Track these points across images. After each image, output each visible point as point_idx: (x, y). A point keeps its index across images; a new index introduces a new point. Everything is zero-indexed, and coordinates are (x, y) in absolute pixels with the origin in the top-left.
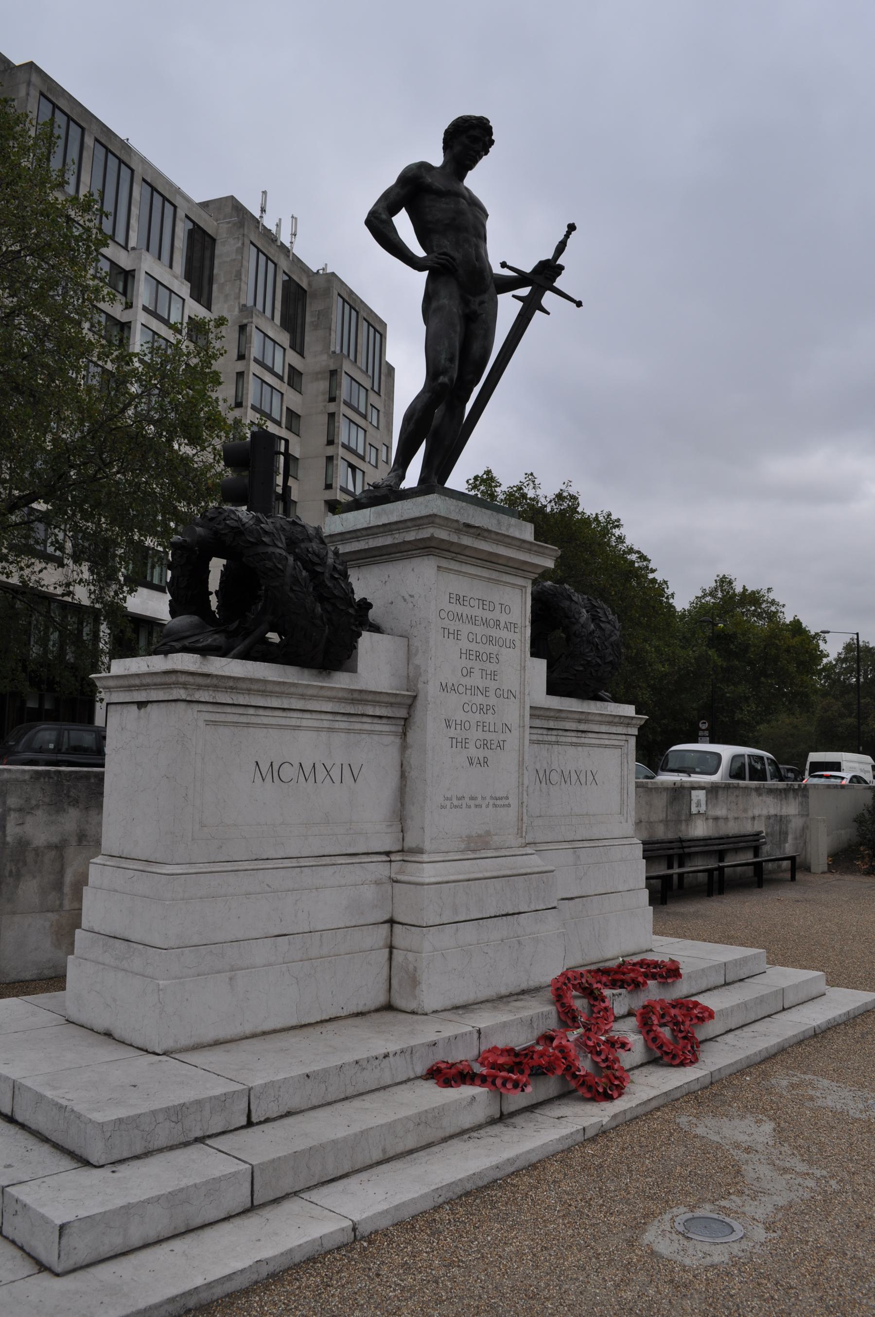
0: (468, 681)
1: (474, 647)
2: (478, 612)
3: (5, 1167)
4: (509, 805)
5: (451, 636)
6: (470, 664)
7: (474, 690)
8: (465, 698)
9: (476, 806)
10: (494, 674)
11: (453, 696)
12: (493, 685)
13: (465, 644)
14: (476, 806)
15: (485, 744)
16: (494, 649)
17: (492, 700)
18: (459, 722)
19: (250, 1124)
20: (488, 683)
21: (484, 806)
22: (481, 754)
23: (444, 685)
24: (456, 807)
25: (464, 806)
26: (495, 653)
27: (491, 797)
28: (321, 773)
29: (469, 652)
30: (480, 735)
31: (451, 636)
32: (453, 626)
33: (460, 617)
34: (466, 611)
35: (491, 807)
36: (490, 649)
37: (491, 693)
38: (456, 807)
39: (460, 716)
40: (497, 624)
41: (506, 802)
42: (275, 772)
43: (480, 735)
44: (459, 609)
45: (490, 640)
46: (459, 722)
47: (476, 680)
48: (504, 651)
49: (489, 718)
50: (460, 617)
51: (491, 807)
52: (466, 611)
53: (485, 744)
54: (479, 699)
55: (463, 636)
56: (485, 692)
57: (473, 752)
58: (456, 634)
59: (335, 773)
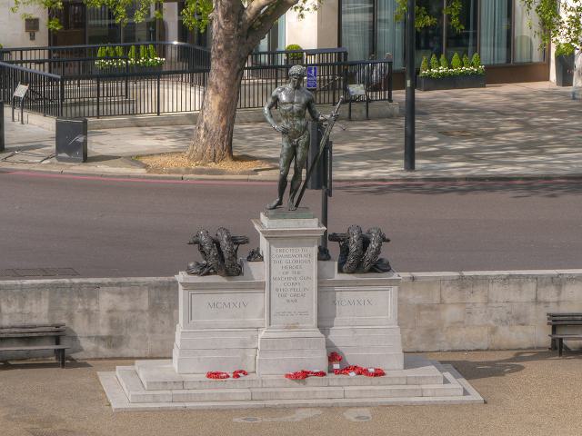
57: (288, 297)
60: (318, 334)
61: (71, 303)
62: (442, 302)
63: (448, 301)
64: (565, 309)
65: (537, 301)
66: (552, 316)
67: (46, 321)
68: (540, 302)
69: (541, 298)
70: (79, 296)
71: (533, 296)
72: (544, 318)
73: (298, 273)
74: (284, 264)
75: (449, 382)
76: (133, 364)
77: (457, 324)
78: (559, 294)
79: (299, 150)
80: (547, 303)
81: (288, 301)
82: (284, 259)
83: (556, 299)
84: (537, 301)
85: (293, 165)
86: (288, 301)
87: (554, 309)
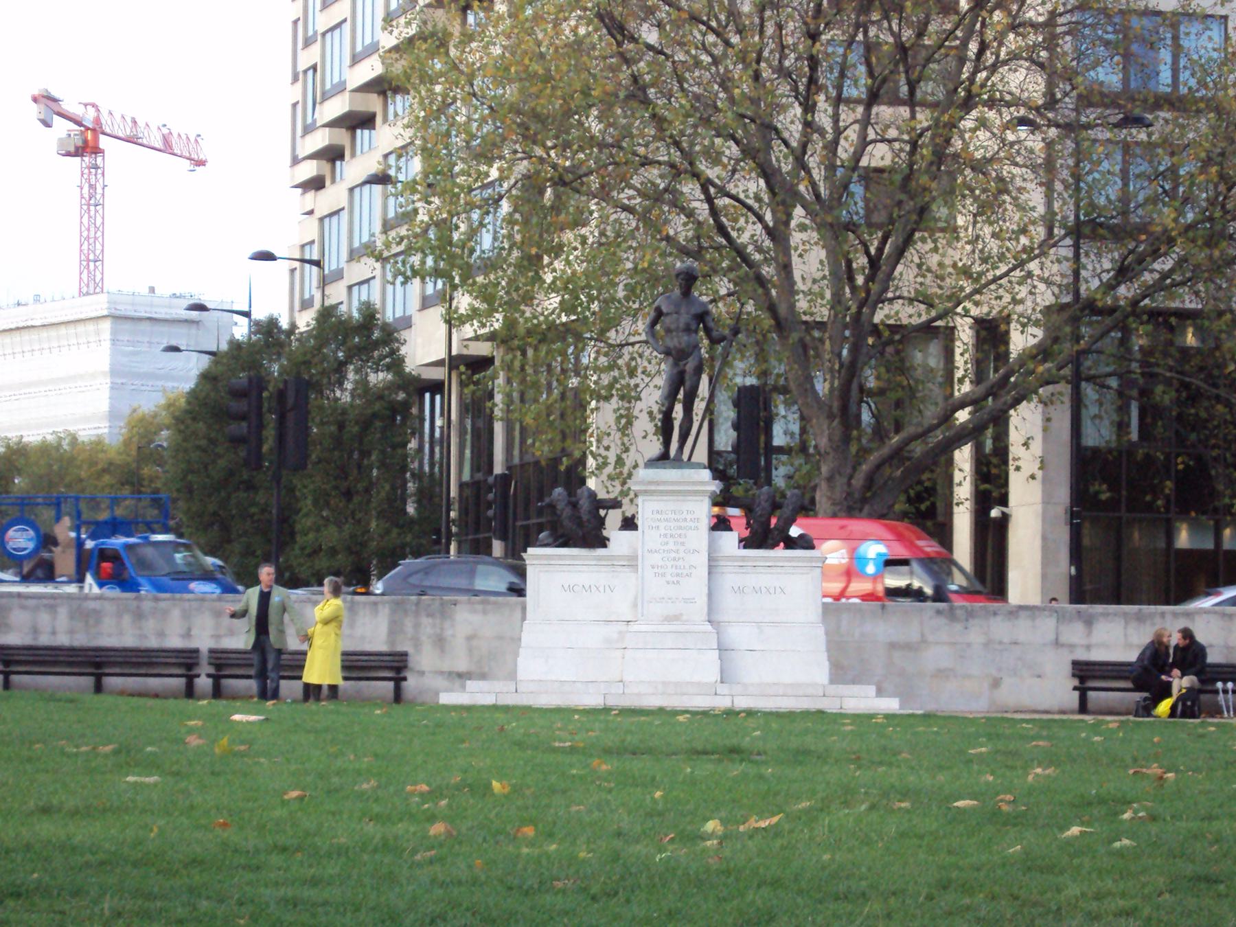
0: (666, 548)
1: (669, 532)
12: (682, 548)
15: (678, 575)
17: (682, 554)
28: (594, 589)
29: (665, 535)
45: (680, 528)
47: (671, 546)
49: (680, 563)
53: (678, 575)
54: (673, 555)
57: (669, 578)
59: (601, 589)
60: (709, 627)
61: (417, 626)
62: (924, 640)
63: (930, 638)
64: (1098, 655)
65: (1057, 643)
66: (1076, 664)
67: (382, 647)
68: (1063, 645)
69: (1064, 639)
70: (428, 615)
71: (1053, 637)
72: (1067, 669)
73: (683, 544)
74: (663, 531)
75: (1028, 448)
76: (463, 687)
77: (942, 674)
78: (1089, 634)
79: (687, 377)
80: (1072, 647)
82: (662, 525)
83: (1084, 642)
84: (1057, 643)
85: (681, 396)
87: (1082, 656)
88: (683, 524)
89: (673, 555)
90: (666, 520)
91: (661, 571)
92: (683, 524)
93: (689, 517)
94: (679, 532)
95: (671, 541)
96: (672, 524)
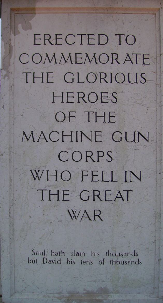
0: (67, 127)
1: (75, 88)
2: (84, 49)
3: (31, 218)
4: (139, 262)
5: (38, 81)
6: (67, 108)
7: (75, 136)
8: (61, 146)
9: (83, 262)
10: (109, 117)
11: (44, 146)
12: (107, 129)
13: (59, 87)
14: (83, 262)
15: (96, 195)
16: (109, 88)
17: (107, 144)
18: (52, 172)
19: (128, 191)
20: (100, 126)
21: (95, 263)
22: (90, 206)
23: (28, 134)
24: (51, 262)
25: (64, 261)
26: (110, 92)
27: (108, 254)
29: (66, 97)
30: (88, 184)
31: (38, 81)
32: (39, 70)
33: (52, 59)
34: (58, 50)
35: (107, 263)
36: (99, 87)
37: (106, 138)
38: (51, 262)
39: (55, 165)
40: (114, 58)
41: (135, 259)
42: (140, 124)
43: (88, 184)
44: (50, 49)
45: (102, 77)
46: (52, 172)
47: (80, 123)
48: (126, 86)
49: (103, 165)
50: (52, 59)
51: (107, 263)
52: (58, 50)
53: (96, 195)
54: (86, 145)
55: (57, 79)
56: (95, 137)
57: (75, 204)
58: (47, 78)
73: (109, 117)
81: (73, 215)
86: (73, 215)
88: (109, 68)
89: (86, 145)
90: (72, 59)
91: (53, 185)
92: (109, 68)
93: (123, 50)
94: (99, 87)
95: (80, 109)
96: (84, 69)
